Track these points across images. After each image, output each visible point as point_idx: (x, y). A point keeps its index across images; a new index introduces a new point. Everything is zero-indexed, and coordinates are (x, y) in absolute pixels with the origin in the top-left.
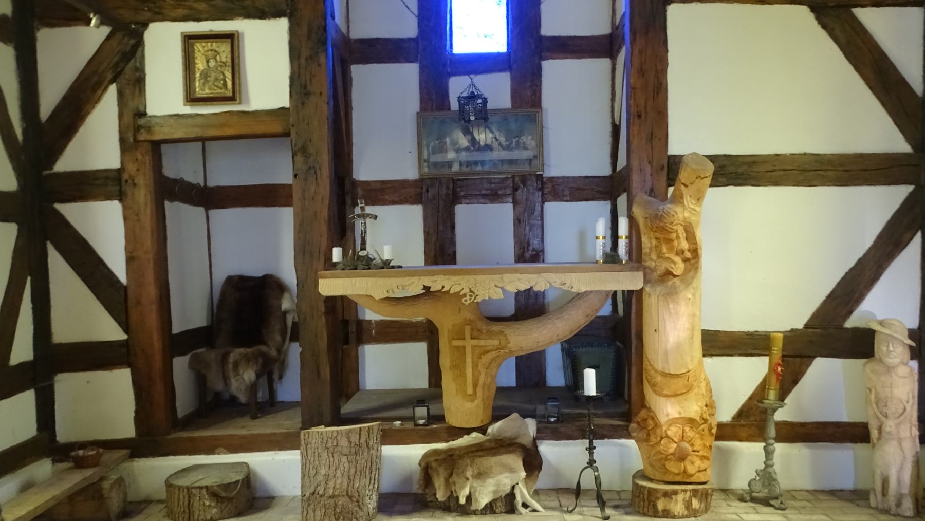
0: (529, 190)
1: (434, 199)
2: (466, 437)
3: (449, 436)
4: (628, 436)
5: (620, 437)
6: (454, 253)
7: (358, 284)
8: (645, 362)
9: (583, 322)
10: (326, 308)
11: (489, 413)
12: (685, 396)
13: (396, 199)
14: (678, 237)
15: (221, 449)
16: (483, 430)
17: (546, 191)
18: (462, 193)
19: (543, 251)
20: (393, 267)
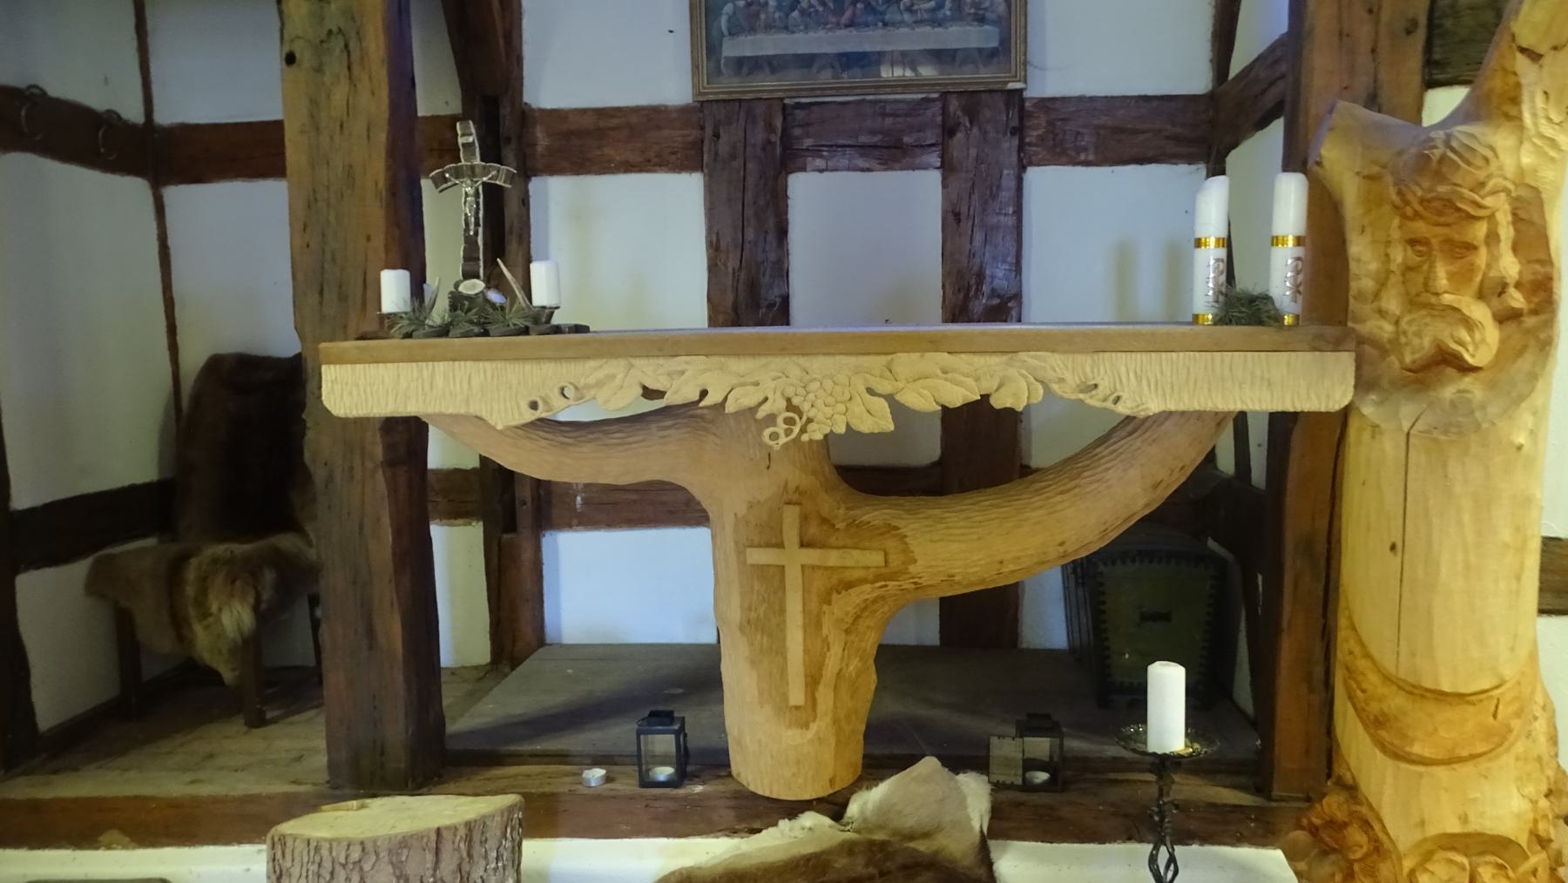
0: (984, 133)
1: (733, 157)
2: (784, 824)
3: (740, 819)
4: (1263, 835)
5: (1238, 840)
6: (786, 300)
7: (439, 381)
8: (1345, 644)
9: (1141, 502)
10: (389, 447)
11: (855, 752)
12: (1483, 764)
13: (634, 158)
14: (1492, 238)
15: (114, 835)
16: (834, 806)
17: (1032, 136)
18: (808, 142)
19: (1018, 297)
20: (557, 330)
